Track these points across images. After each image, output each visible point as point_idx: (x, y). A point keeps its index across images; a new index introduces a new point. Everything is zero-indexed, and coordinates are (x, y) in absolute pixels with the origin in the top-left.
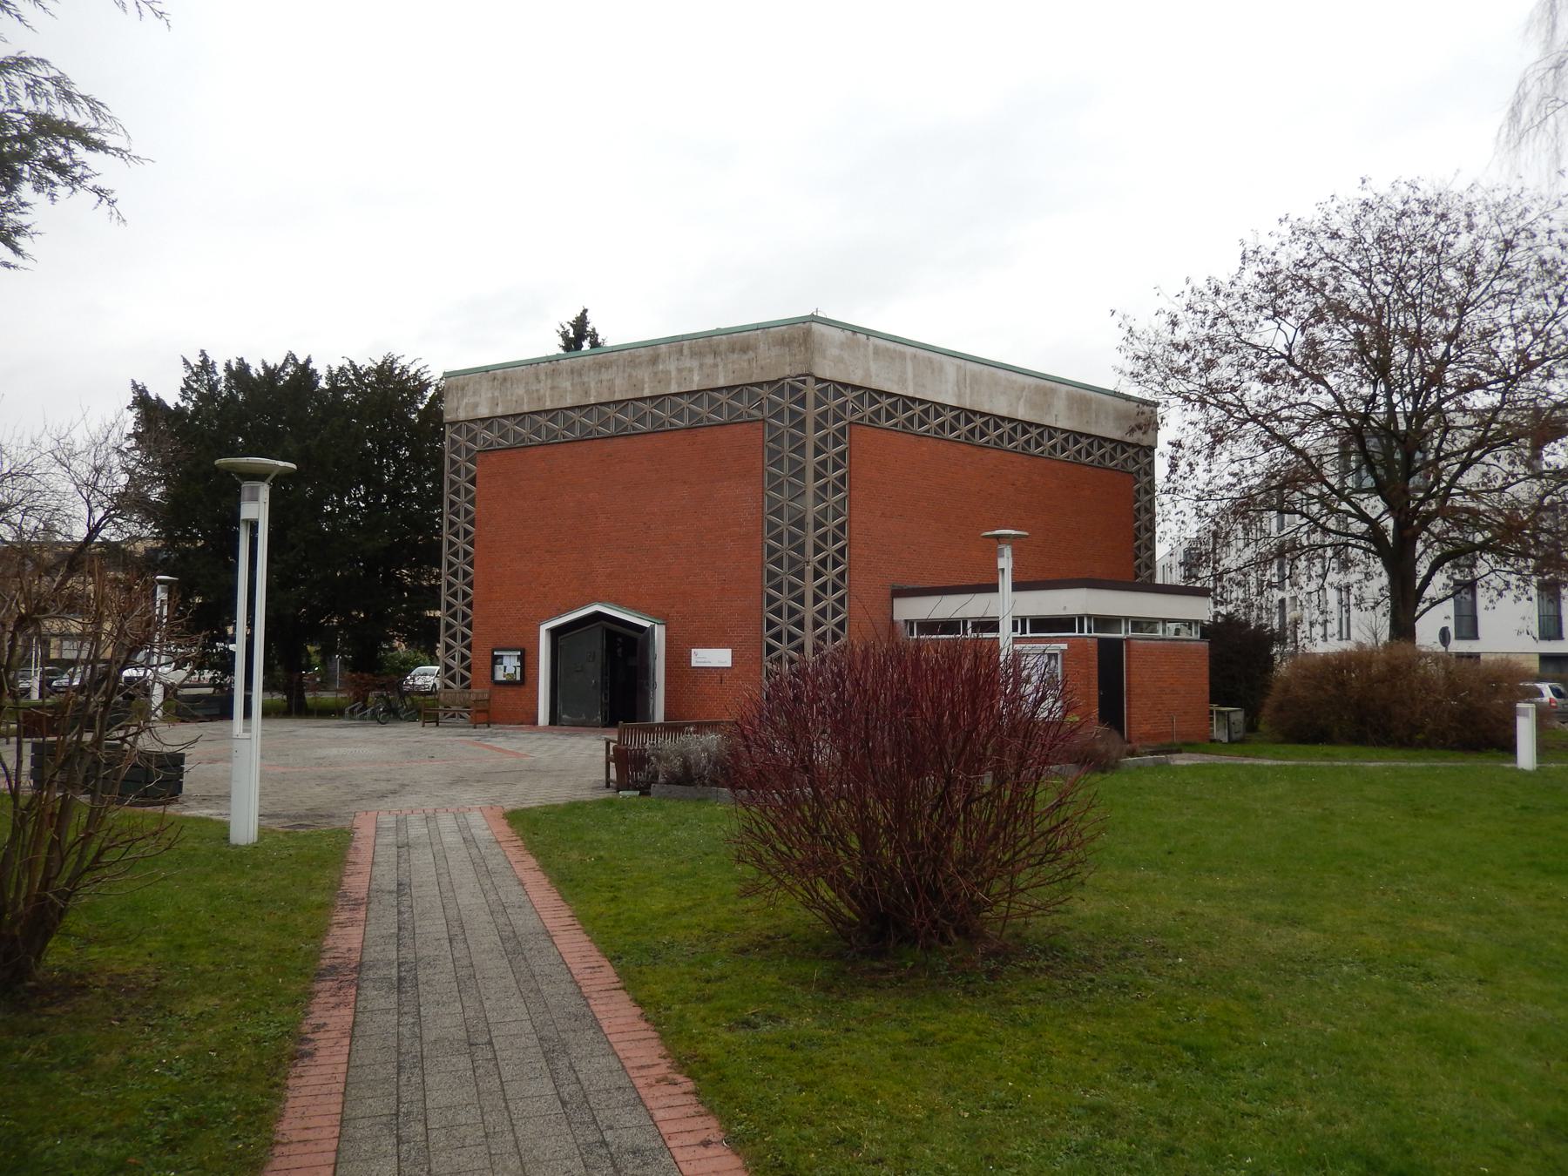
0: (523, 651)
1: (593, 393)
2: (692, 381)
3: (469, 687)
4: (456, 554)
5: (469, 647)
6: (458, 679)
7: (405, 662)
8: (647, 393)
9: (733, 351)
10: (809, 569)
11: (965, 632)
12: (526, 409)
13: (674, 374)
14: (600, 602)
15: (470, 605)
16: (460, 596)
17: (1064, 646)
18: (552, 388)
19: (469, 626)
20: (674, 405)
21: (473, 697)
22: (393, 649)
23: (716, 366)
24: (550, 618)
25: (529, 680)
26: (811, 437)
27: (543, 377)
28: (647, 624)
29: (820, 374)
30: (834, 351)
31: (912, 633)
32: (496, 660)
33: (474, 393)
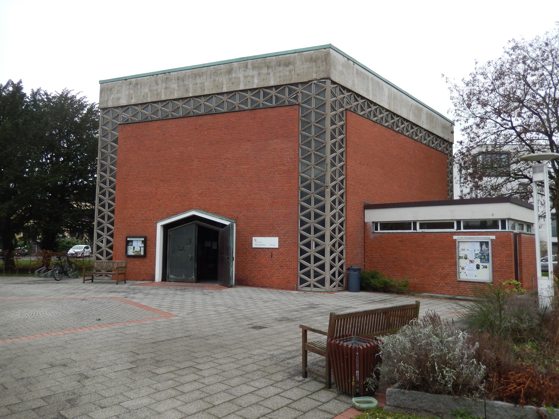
0: (146, 238)
1: (191, 90)
2: (253, 83)
3: (111, 259)
4: (104, 183)
5: (112, 236)
6: (105, 253)
7: (68, 243)
8: (225, 90)
9: (280, 66)
10: (328, 191)
11: (415, 228)
12: (149, 100)
13: (242, 79)
14: (195, 209)
15: (113, 212)
16: (107, 206)
17: (493, 237)
18: (166, 88)
19: (112, 224)
20: (241, 97)
21: (115, 266)
22: (64, 237)
23: (268, 74)
25: (149, 255)
26: (329, 114)
27: (160, 82)
28: (227, 223)
29: (334, 79)
30: (340, 68)
31: (376, 229)
32: (128, 243)
33: (118, 92)
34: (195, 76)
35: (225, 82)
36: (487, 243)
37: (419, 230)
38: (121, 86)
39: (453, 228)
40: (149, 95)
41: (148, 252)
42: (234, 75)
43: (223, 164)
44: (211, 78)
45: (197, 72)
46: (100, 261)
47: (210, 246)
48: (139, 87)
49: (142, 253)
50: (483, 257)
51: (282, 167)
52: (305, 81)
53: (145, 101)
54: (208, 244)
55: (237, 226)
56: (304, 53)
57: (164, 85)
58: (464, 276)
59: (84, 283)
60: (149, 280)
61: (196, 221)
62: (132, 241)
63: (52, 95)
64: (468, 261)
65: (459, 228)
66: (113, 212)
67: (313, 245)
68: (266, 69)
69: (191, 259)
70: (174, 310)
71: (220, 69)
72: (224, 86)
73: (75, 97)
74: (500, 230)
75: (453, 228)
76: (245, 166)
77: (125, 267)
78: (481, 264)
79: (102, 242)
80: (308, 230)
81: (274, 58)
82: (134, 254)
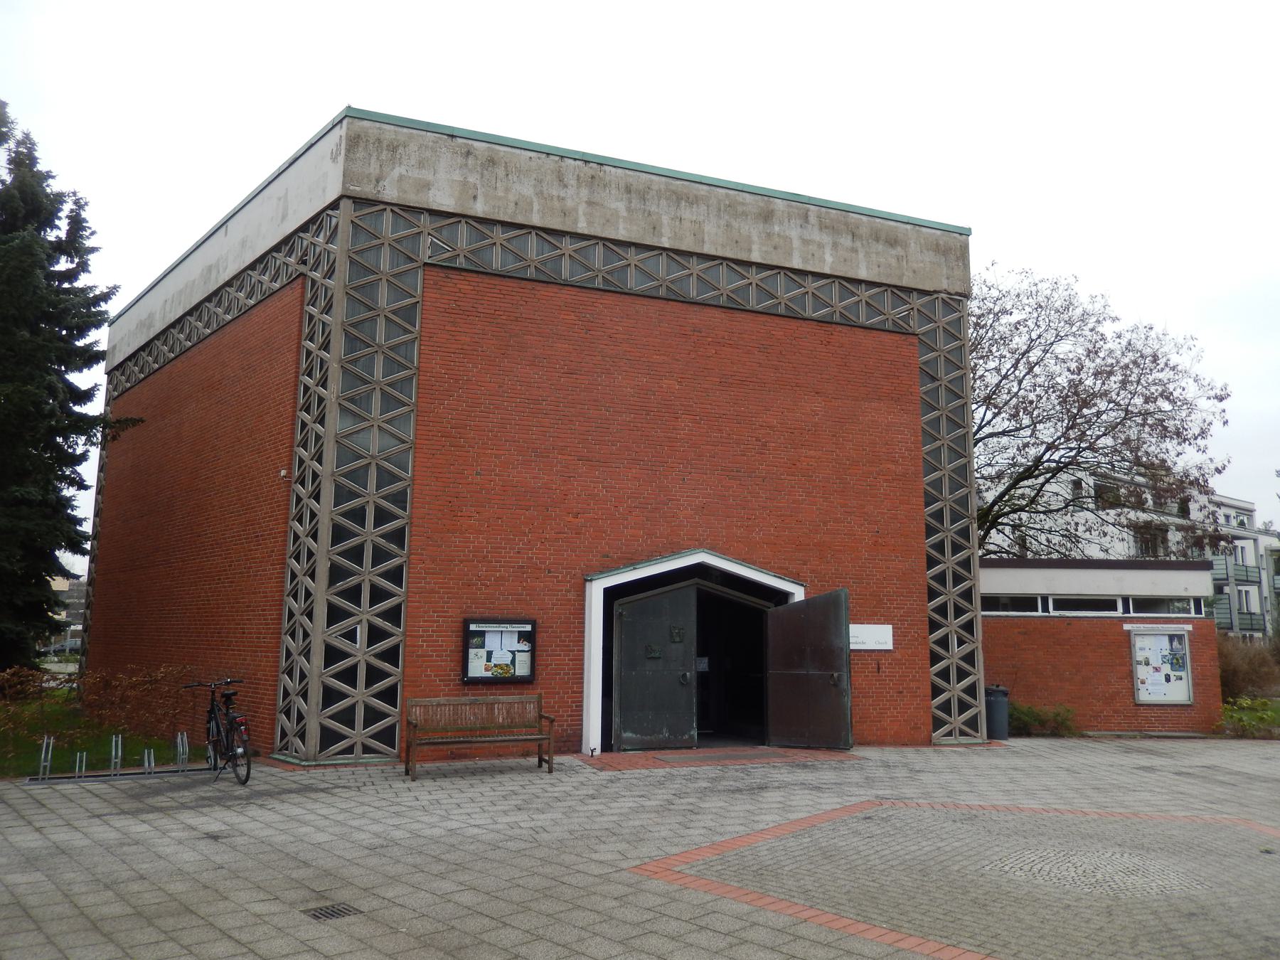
1: (666, 231)
9: (877, 240)
11: (1045, 609)
14: (700, 545)
17: (1190, 627)
32: (468, 639)
34: (678, 198)
35: (755, 238)
36: (1180, 637)
37: (1053, 613)
38: (433, 150)
39: (1115, 609)
40: (536, 207)
42: (777, 228)
44: (719, 216)
45: (767, 205)
48: (501, 172)
49: (522, 669)
50: (1176, 662)
51: (893, 467)
52: (927, 288)
53: (520, 219)
56: (924, 230)
57: (584, 192)
58: (1144, 696)
61: (696, 580)
64: (1150, 669)
65: (1126, 610)
67: (362, 634)
68: (850, 237)
71: (743, 204)
72: (755, 247)
74: (1193, 614)
75: (1115, 609)
78: (1172, 674)
80: (378, 595)
81: (864, 218)
82: (489, 674)
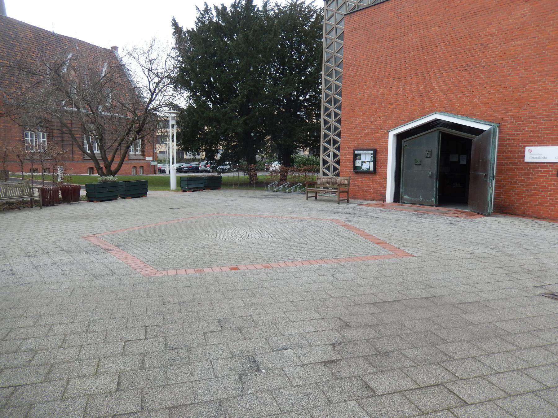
5: (338, 149)
6: (331, 169)
14: (439, 112)
15: (339, 121)
24: (396, 126)
25: (379, 170)
28: (486, 128)
41: (378, 168)
43: (482, 44)
46: (327, 177)
47: (457, 160)
49: (371, 169)
54: (454, 158)
55: (499, 132)
59: (307, 200)
60: (379, 200)
62: (360, 155)
63: (283, 5)
66: (339, 121)
69: (431, 177)
70: (408, 244)
73: (304, 3)
76: (519, 42)
77: (348, 184)
79: (329, 156)
